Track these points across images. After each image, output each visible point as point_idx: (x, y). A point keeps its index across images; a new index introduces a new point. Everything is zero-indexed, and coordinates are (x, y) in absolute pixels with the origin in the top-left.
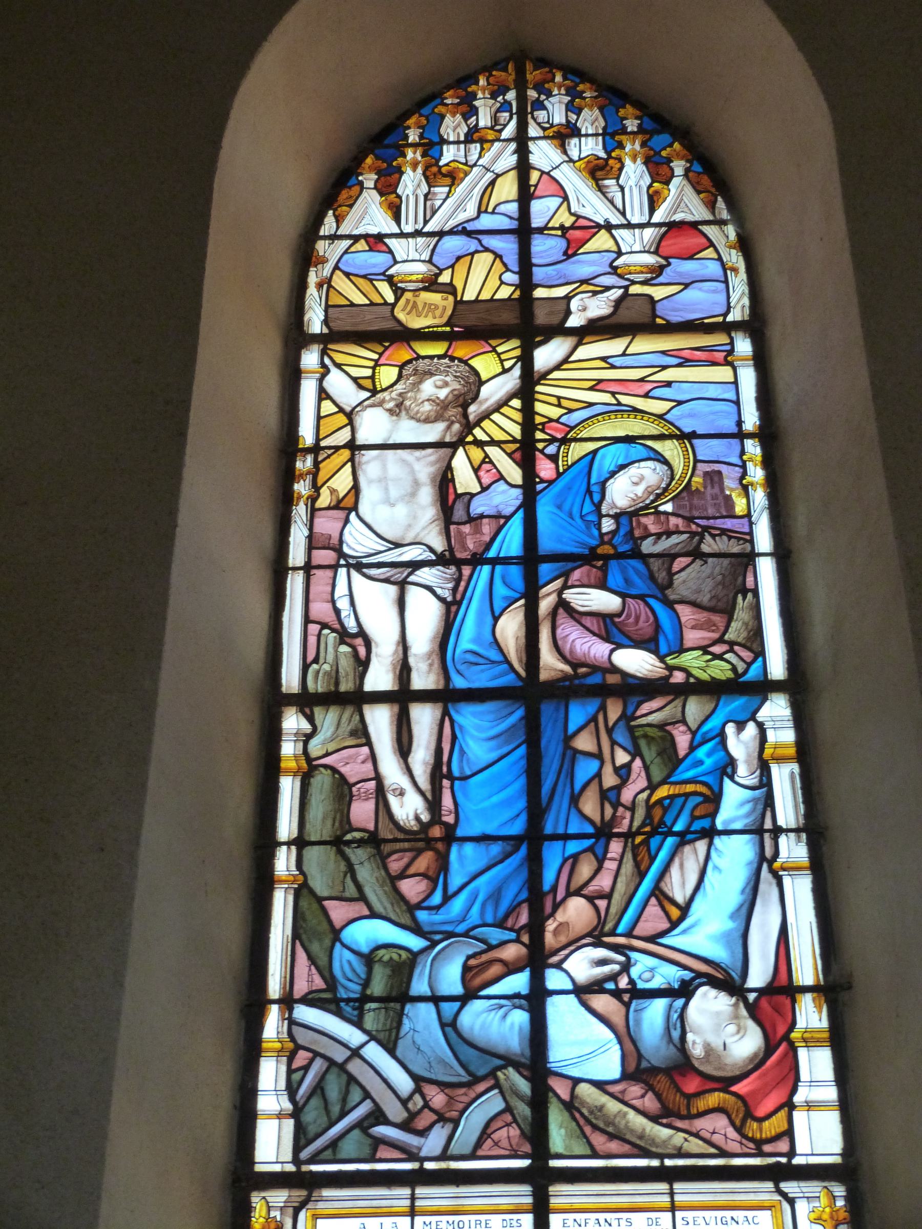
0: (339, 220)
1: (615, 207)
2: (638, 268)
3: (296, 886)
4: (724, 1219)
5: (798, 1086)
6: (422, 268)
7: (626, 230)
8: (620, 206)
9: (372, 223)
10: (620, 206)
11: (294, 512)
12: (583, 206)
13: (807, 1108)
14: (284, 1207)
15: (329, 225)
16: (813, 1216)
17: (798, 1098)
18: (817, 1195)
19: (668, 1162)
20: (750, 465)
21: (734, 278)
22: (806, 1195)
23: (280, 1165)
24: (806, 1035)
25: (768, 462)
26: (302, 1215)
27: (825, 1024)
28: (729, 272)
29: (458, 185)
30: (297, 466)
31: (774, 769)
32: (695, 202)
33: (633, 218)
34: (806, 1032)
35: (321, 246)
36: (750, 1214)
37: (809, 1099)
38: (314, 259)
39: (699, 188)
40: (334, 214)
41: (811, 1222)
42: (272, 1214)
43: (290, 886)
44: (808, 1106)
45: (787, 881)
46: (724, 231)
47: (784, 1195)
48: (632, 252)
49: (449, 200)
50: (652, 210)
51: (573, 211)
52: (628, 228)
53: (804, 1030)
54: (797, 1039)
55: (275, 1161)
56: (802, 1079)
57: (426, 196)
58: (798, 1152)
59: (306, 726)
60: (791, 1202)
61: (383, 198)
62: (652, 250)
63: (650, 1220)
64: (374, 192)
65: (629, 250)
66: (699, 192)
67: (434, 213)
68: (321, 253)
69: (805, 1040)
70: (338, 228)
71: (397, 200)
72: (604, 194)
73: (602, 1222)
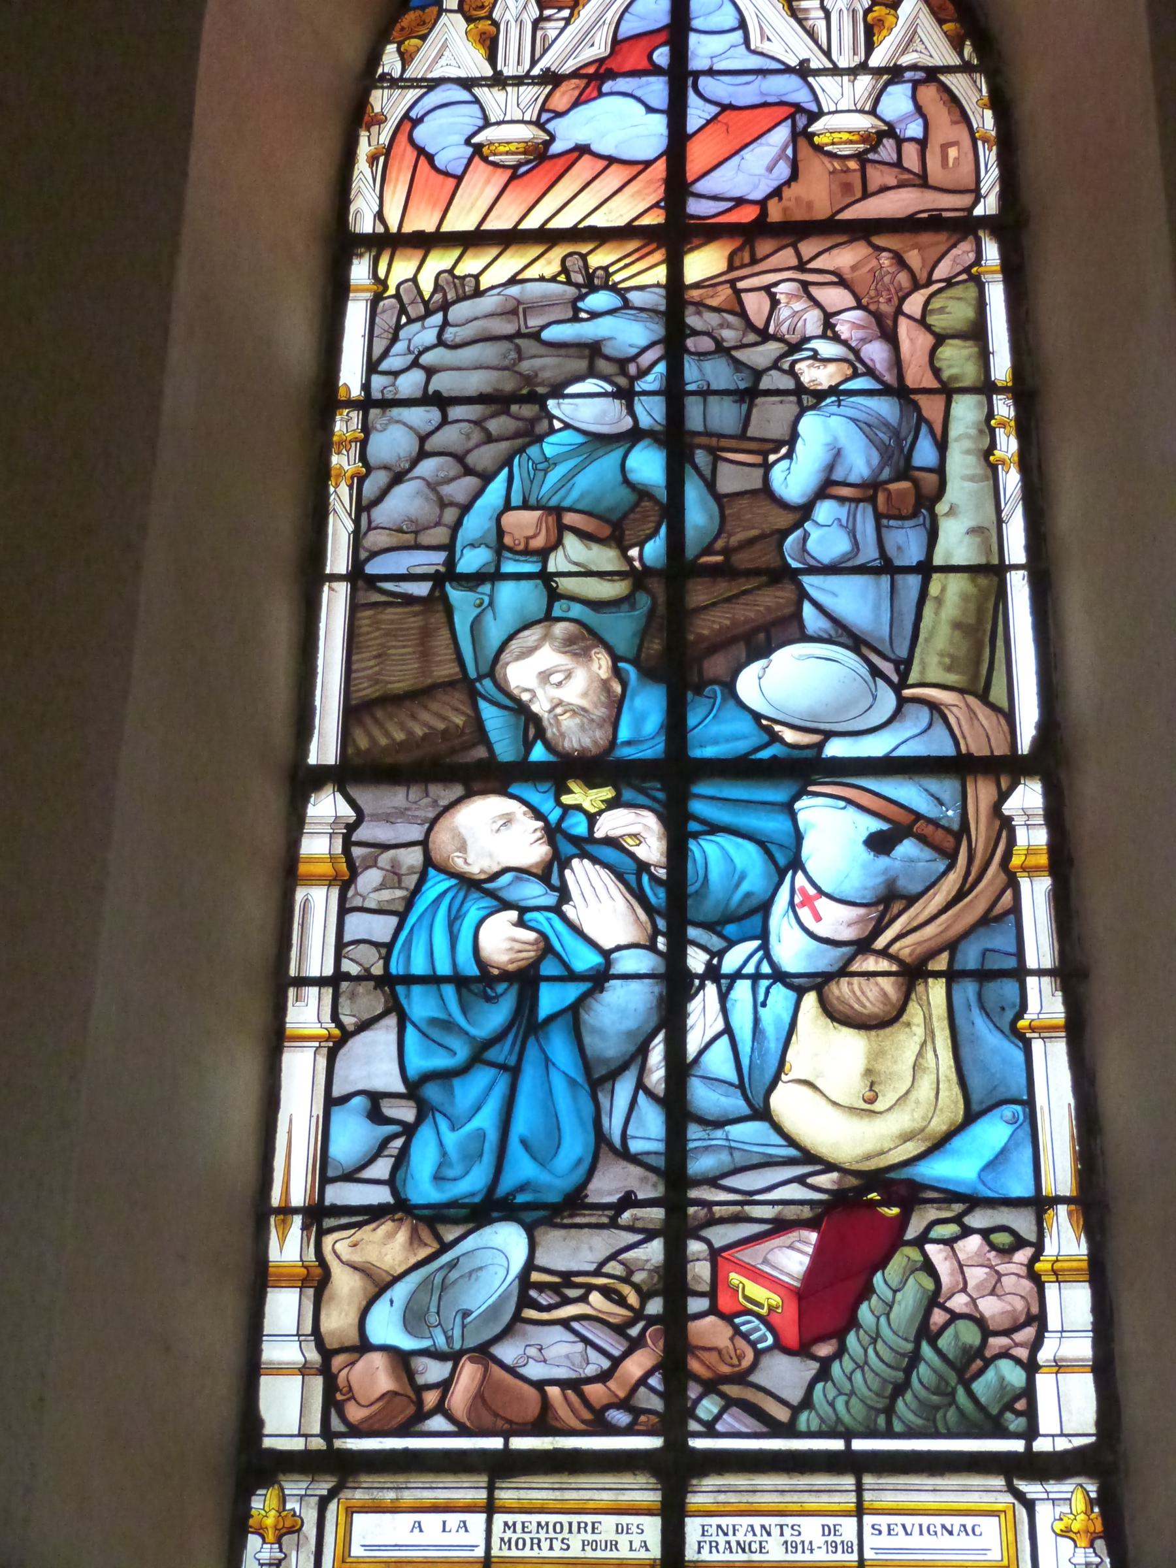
0: (406, 59)
1: (816, 42)
2: (845, 136)
3: (331, 1044)
4: (932, 1528)
5: (1044, 1337)
6: (527, 133)
7: (830, 78)
8: (825, 47)
9: (453, 63)
10: (825, 47)
11: (332, 498)
12: (769, 39)
13: (1055, 1369)
14: (306, 1495)
15: (390, 62)
16: (1059, 1526)
17: (1044, 1356)
18: (1068, 1495)
19: (858, 1445)
20: (1000, 434)
21: (987, 152)
22: (1052, 1496)
23: (302, 1440)
24: (1057, 1266)
25: (1025, 429)
26: (333, 1506)
27: (1083, 1249)
28: (980, 143)
29: (584, 6)
30: (337, 429)
31: (1024, 883)
32: (935, 37)
33: (841, 58)
34: (1057, 1261)
35: (379, 99)
36: (969, 1521)
37: (1060, 1354)
38: (366, 118)
39: (941, 16)
40: (399, 50)
41: (1057, 1534)
42: (289, 1506)
43: (323, 1044)
44: (1057, 1365)
45: (1037, 1046)
46: (975, 82)
47: (1020, 1496)
48: (836, 112)
49: (570, 29)
50: (870, 48)
51: (753, 47)
52: (833, 75)
53: (1055, 1258)
54: (1046, 1271)
55: (296, 1432)
56: (1051, 1327)
57: (536, 24)
58: (1042, 1431)
59: (347, 812)
60: (1030, 1505)
61: (472, 26)
62: (867, 108)
63: (826, 1528)
64: (459, 16)
65: (833, 108)
66: (941, 22)
67: (545, 51)
68: (377, 109)
69: (1055, 1272)
70: (404, 70)
71: (493, 29)
72: (800, 22)
73: (758, 1530)
